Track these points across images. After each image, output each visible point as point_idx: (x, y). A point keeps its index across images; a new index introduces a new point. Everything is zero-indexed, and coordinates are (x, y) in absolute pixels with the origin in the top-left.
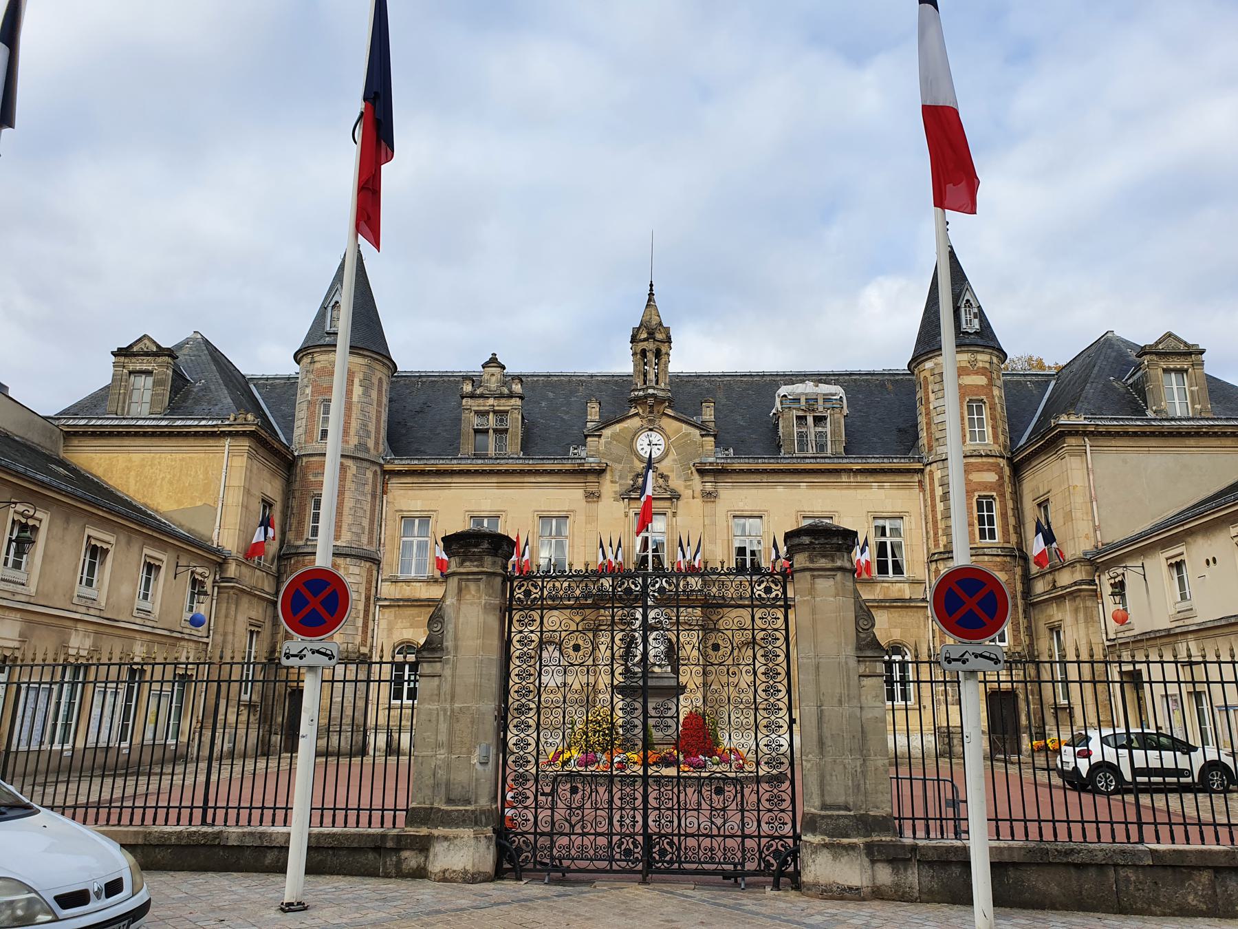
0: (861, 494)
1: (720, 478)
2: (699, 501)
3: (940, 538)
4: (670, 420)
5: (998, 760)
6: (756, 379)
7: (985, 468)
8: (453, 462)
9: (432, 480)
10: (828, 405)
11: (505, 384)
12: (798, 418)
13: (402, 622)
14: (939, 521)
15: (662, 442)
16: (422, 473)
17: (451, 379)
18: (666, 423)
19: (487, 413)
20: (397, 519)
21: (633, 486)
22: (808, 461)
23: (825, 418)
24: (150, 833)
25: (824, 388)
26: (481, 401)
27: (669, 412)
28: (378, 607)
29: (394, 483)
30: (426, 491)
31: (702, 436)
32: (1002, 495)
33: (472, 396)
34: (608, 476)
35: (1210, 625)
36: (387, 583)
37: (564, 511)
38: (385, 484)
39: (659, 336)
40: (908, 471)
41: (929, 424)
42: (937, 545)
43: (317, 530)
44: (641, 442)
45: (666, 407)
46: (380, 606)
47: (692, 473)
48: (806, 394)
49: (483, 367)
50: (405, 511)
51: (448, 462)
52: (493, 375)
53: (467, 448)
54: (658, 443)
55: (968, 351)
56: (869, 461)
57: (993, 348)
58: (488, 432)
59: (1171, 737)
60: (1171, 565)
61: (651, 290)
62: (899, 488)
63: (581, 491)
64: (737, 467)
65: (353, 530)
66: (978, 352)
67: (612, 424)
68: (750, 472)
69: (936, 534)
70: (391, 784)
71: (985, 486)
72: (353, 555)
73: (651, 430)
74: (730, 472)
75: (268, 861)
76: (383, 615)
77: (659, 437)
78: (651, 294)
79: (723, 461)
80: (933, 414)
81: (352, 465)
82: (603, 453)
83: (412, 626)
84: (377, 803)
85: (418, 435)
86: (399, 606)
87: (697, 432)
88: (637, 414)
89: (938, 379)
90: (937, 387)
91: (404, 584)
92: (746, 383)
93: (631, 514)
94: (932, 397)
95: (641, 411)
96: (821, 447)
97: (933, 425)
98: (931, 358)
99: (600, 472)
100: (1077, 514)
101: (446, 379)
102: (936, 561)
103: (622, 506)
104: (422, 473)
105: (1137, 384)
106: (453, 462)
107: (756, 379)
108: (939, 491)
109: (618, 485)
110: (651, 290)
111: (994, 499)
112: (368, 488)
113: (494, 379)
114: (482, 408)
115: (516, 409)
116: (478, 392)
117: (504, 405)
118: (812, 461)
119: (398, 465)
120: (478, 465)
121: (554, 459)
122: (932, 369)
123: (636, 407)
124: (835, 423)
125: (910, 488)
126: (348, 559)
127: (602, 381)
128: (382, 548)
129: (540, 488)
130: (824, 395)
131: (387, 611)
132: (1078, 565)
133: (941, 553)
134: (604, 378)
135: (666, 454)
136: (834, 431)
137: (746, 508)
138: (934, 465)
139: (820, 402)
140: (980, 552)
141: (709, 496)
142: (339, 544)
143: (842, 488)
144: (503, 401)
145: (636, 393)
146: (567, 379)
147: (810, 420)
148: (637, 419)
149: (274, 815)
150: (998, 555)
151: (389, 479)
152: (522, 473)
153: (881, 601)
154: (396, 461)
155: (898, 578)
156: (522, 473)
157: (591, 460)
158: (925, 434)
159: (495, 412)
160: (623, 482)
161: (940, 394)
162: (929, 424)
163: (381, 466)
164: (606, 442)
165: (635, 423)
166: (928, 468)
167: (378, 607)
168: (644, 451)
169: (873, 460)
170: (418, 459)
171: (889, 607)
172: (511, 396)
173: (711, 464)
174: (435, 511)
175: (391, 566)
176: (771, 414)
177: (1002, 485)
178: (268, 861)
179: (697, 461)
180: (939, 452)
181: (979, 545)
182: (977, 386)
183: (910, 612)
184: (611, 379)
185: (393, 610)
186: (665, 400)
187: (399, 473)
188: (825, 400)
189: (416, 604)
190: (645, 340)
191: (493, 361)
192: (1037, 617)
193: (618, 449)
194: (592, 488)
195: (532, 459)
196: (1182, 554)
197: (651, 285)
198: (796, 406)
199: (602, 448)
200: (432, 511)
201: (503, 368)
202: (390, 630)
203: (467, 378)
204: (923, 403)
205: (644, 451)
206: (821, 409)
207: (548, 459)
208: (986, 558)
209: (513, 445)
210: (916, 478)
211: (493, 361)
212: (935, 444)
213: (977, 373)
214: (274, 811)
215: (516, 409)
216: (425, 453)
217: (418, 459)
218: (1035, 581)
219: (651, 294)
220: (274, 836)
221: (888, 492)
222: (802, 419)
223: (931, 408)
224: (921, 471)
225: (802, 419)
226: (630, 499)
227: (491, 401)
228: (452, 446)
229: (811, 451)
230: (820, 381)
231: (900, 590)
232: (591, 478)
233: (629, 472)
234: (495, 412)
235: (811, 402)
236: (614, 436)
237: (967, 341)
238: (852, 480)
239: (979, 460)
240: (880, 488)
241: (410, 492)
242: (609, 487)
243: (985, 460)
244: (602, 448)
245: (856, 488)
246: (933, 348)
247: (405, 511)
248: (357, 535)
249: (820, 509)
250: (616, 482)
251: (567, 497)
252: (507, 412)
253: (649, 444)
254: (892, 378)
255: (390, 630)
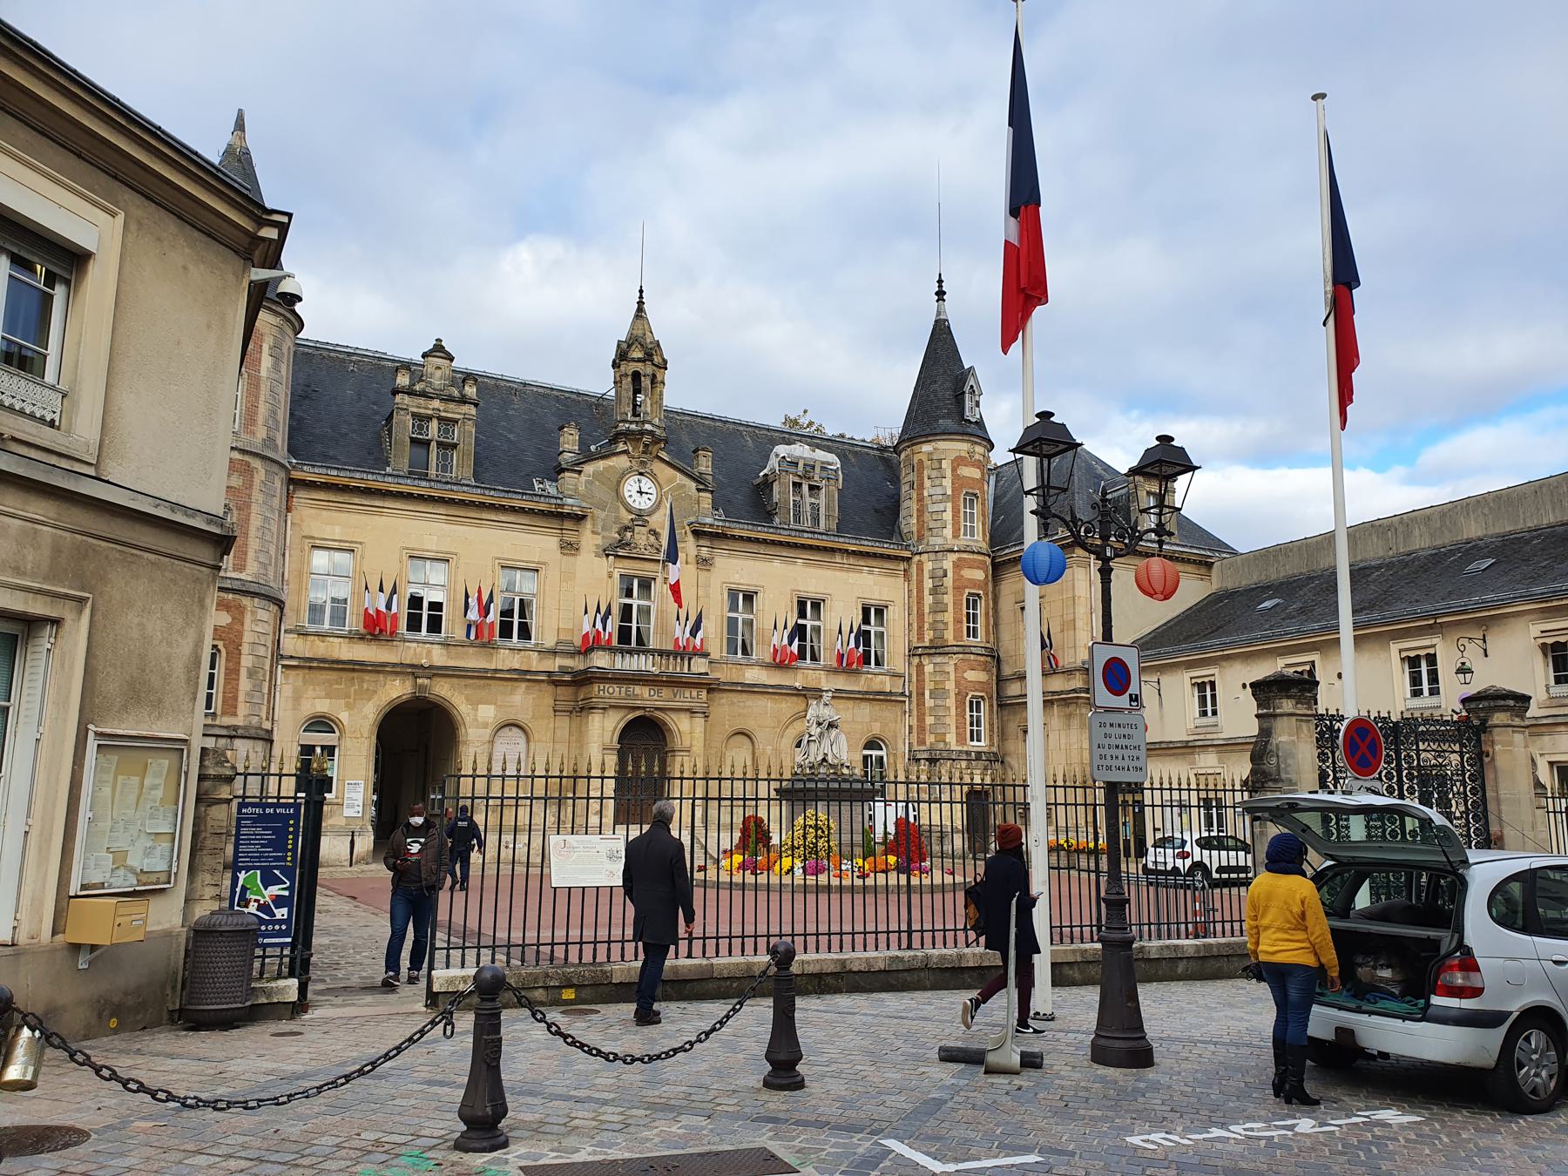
0: (853, 577)
1: (717, 543)
2: (692, 568)
3: (926, 632)
4: (663, 466)
5: (980, 859)
6: (718, 424)
7: (976, 565)
8: (386, 480)
9: (357, 501)
10: (824, 474)
11: (453, 383)
12: (794, 483)
13: (314, 690)
14: (926, 616)
15: (653, 490)
16: (345, 489)
17: (332, 354)
18: (658, 467)
19: (430, 418)
20: (306, 548)
21: (620, 541)
22: (806, 535)
23: (818, 488)
24: (1086, 950)
25: (821, 455)
26: (422, 401)
27: (663, 455)
28: (280, 667)
29: (301, 496)
30: (348, 514)
31: (699, 490)
32: (986, 595)
33: (410, 392)
34: (588, 524)
35: (1240, 741)
36: (292, 636)
37: (533, 562)
38: (289, 497)
39: (657, 359)
40: (897, 558)
41: (921, 512)
42: (921, 637)
43: (799, 613)
44: (629, 488)
45: (661, 449)
46: (283, 666)
47: (686, 533)
48: (804, 458)
49: (424, 355)
50: (318, 539)
51: (379, 478)
52: (438, 368)
53: (401, 460)
54: (649, 491)
55: (968, 441)
56: (863, 542)
57: (984, 439)
58: (429, 444)
59: (1234, 838)
60: (1193, 685)
61: (641, 297)
62: (887, 575)
63: (556, 540)
64: (737, 533)
65: (261, 560)
66: (976, 443)
67: (595, 459)
68: (749, 540)
69: (920, 628)
70: (504, 904)
71: (974, 583)
72: (263, 595)
73: (641, 474)
74: (728, 538)
75: (1180, 970)
76: (287, 678)
77: (650, 484)
78: (641, 303)
79: (721, 524)
80: (928, 501)
81: (260, 468)
82: (584, 495)
83: (328, 696)
84: (724, 931)
85: (317, 431)
86: (310, 668)
87: (693, 485)
88: (626, 452)
89: (936, 465)
90: (934, 474)
91: (316, 638)
92: (709, 427)
93: (616, 576)
94: (927, 483)
95: (631, 449)
96: (816, 520)
97: (926, 513)
98: (930, 441)
99: (579, 519)
100: (1079, 624)
101: (325, 353)
102: (920, 655)
103: (605, 564)
104: (345, 489)
105: (1118, 501)
106: (386, 480)
107: (718, 424)
108: (928, 584)
109: (600, 537)
110: (641, 297)
111: (980, 598)
112: (276, 502)
113: (438, 373)
114: (422, 411)
115: (469, 419)
116: (418, 387)
117: (454, 411)
118: (810, 535)
119: (309, 473)
120: (421, 488)
121: (523, 494)
122: (930, 454)
123: (625, 443)
124: (828, 495)
125: (897, 576)
126: (256, 600)
127: (539, 394)
128: (285, 587)
129: (502, 528)
130: (823, 463)
131: (292, 673)
132: (1078, 673)
133: (926, 647)
134: (540, 390)
135: (657, 506)
136: (826, 502)
137: (742, 581)
138: (925, 557)
139: (817, 470)
140: (967, 650)
141: (704, 563)
142: (243, 578)
143: (835, 569)
144: (452, 406)
145: (627, 425)
146: (493, 382)
147: (805, 488)
148: (624, 458)
149: (934, 937)
150: (982, 655)
151: (294, 491)
152: (482, 506)
153: (867, 693)
154: (305, 468)
155: (434, 637)
156: (482, 506)
157: (570, 501)
158: (915, 521)
159: (440, 419)
160: (607, 534)
161: (937, 482)
162: (921, 512)
163: (288, 471)
164: (586, 481)
165: (621, 462)
166: (917, 558)
167: (280, 667)
168: (632, 499)
169: (866, 543)
170: (338, 469)
171: (861, 699)
172: (463, 400)
173: (711, 526)
174: (361, 543)
175: (298, 611)
176: (762, 474)
177: (987, 584)
178: (1180, 970)
179: (692, 519)
180: (931, 543)
181: (966, 643)
182: (973, 479)
183: (889, 706)
184: (549, 392)
185: (300, 672)
186: (661, 440)
187: (312, 486)
188: (823, 469)
189: (335, 666)
190: (639, 360)
191: (438, 349)
192: (1005, 718)
193: (603, 494)
194: (570, 537)
195: (494, 489)
196: (1214, 675)
197: (641, 291)
198: (794, 470)
199: (582, 488)
200: (356, 542)
201: (452, 359)
202: (297, 698)
203: (406, 366)
204: (915, 487)
205: (632, 499)
206: (817, 478)
207: (515, 493)
208: (972, 657)
209: (461, 466)
210: (902, 566)
211: (438, 349)
212: (927, 533)
213: (973, 466)
214: (463, 951)
215: (469, 419)
216: (334, 458)
217: (338, 469)
218: (1008, 683)
219: (641, 303)
220: (848, 962)
221: (877, 578)
222: (797, 485)
223: (926, 494)
224: (909, 559)
225: (797, 485)
226: (617, 556)
227: (436, 404)
228: (377, 457)
229: (807, 524)
230: (818, 447)
231: (881, 683)
232: (568, 525)
233: (615, 523)
234: (440, 419)
235: (808, 469)
236: (596, 475)
237: (969, 430)
238: (845, 561)
239: (971, 556)
240: (870, 573)
241: (324, 512)
242: (589, 539)
243: (976, 556)
244: (582, 488)
245: (848, 570)
246: (934, 431)
247: (318, 539)
248: (264, 566)
249: (813, 590)
250: (599, 534)
251: (539, 544)
252: (456, 421)
253: (639, 492)
254: (851, 448)
255: (297, 698)
